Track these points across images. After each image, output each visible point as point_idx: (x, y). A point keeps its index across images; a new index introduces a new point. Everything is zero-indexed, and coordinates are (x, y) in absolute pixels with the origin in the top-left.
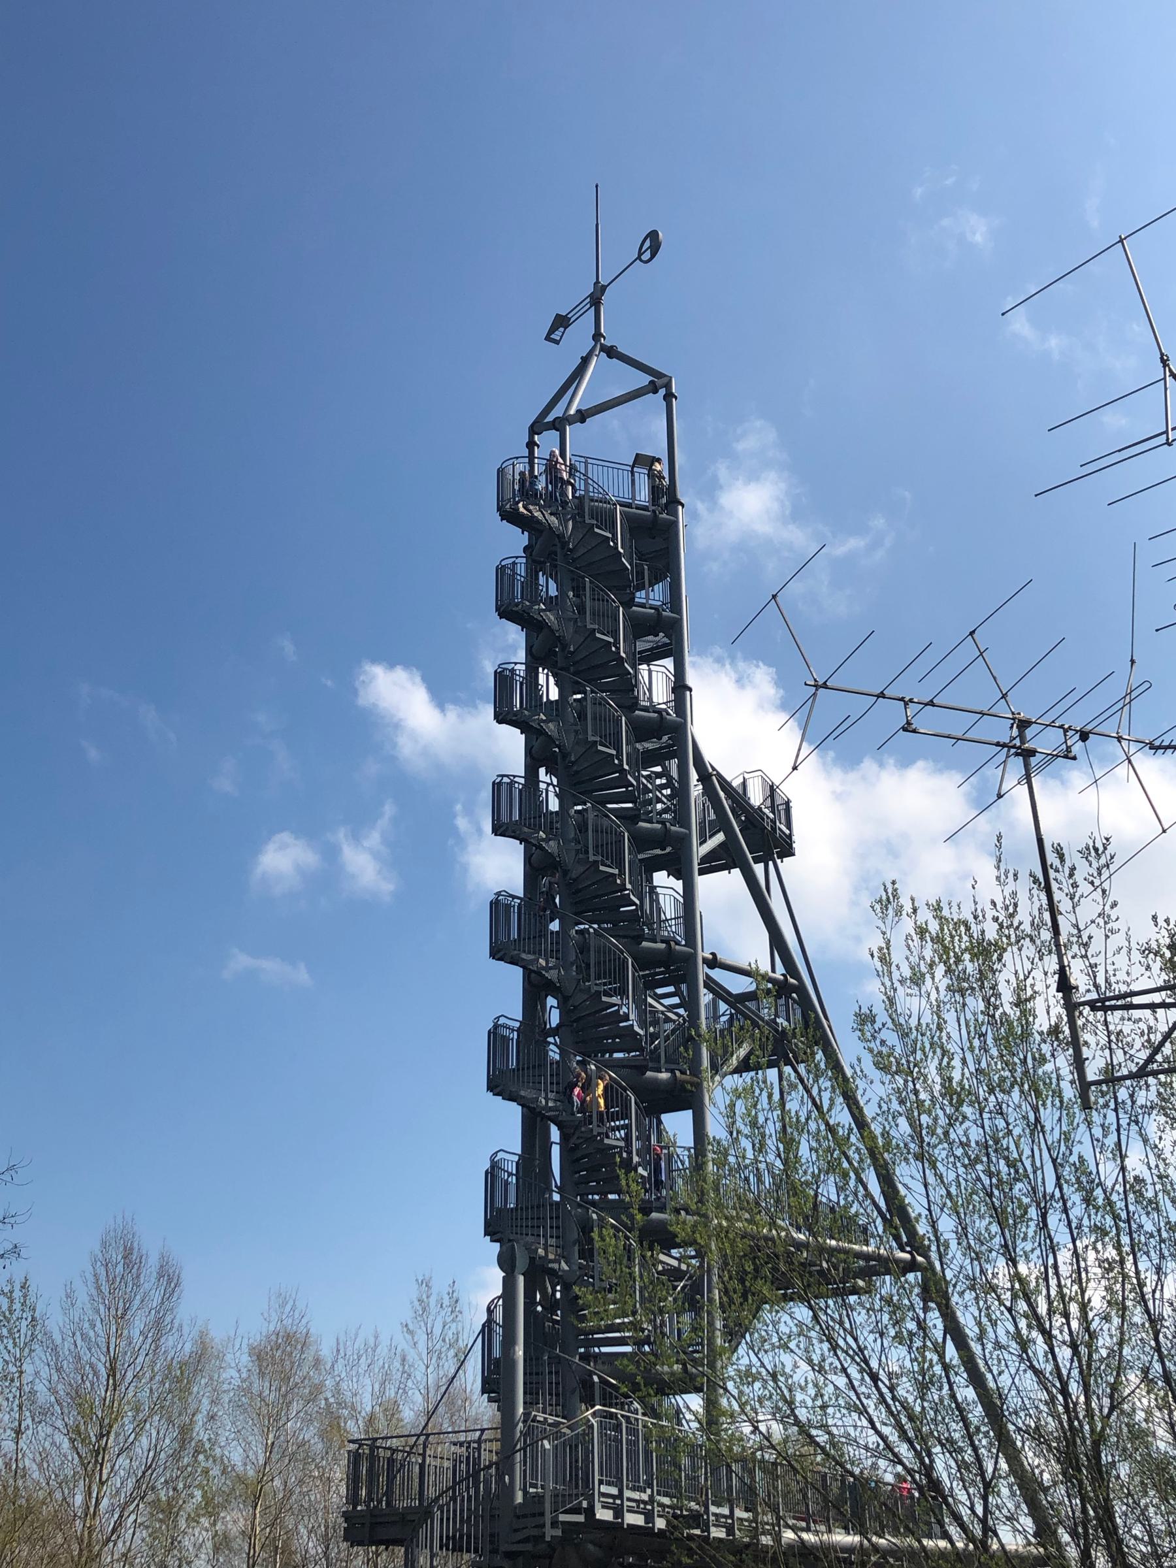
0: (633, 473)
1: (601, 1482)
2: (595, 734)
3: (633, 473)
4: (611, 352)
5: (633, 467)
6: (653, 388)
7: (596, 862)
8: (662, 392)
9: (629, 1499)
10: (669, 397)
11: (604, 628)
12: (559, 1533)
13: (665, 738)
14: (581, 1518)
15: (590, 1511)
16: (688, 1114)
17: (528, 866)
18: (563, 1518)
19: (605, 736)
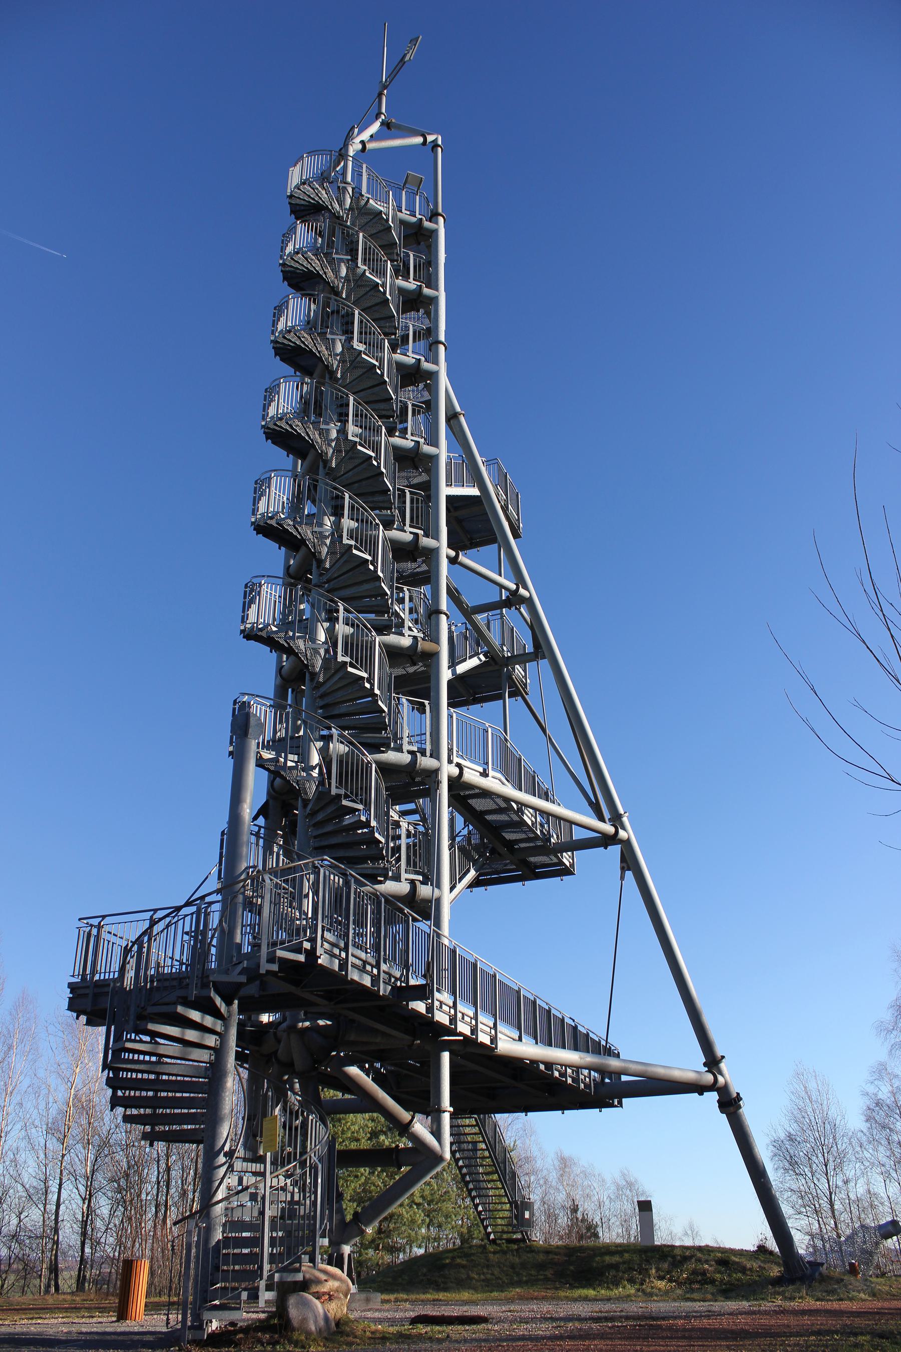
12: (275, 967)
14: (301, 958)
18: (281, 953)
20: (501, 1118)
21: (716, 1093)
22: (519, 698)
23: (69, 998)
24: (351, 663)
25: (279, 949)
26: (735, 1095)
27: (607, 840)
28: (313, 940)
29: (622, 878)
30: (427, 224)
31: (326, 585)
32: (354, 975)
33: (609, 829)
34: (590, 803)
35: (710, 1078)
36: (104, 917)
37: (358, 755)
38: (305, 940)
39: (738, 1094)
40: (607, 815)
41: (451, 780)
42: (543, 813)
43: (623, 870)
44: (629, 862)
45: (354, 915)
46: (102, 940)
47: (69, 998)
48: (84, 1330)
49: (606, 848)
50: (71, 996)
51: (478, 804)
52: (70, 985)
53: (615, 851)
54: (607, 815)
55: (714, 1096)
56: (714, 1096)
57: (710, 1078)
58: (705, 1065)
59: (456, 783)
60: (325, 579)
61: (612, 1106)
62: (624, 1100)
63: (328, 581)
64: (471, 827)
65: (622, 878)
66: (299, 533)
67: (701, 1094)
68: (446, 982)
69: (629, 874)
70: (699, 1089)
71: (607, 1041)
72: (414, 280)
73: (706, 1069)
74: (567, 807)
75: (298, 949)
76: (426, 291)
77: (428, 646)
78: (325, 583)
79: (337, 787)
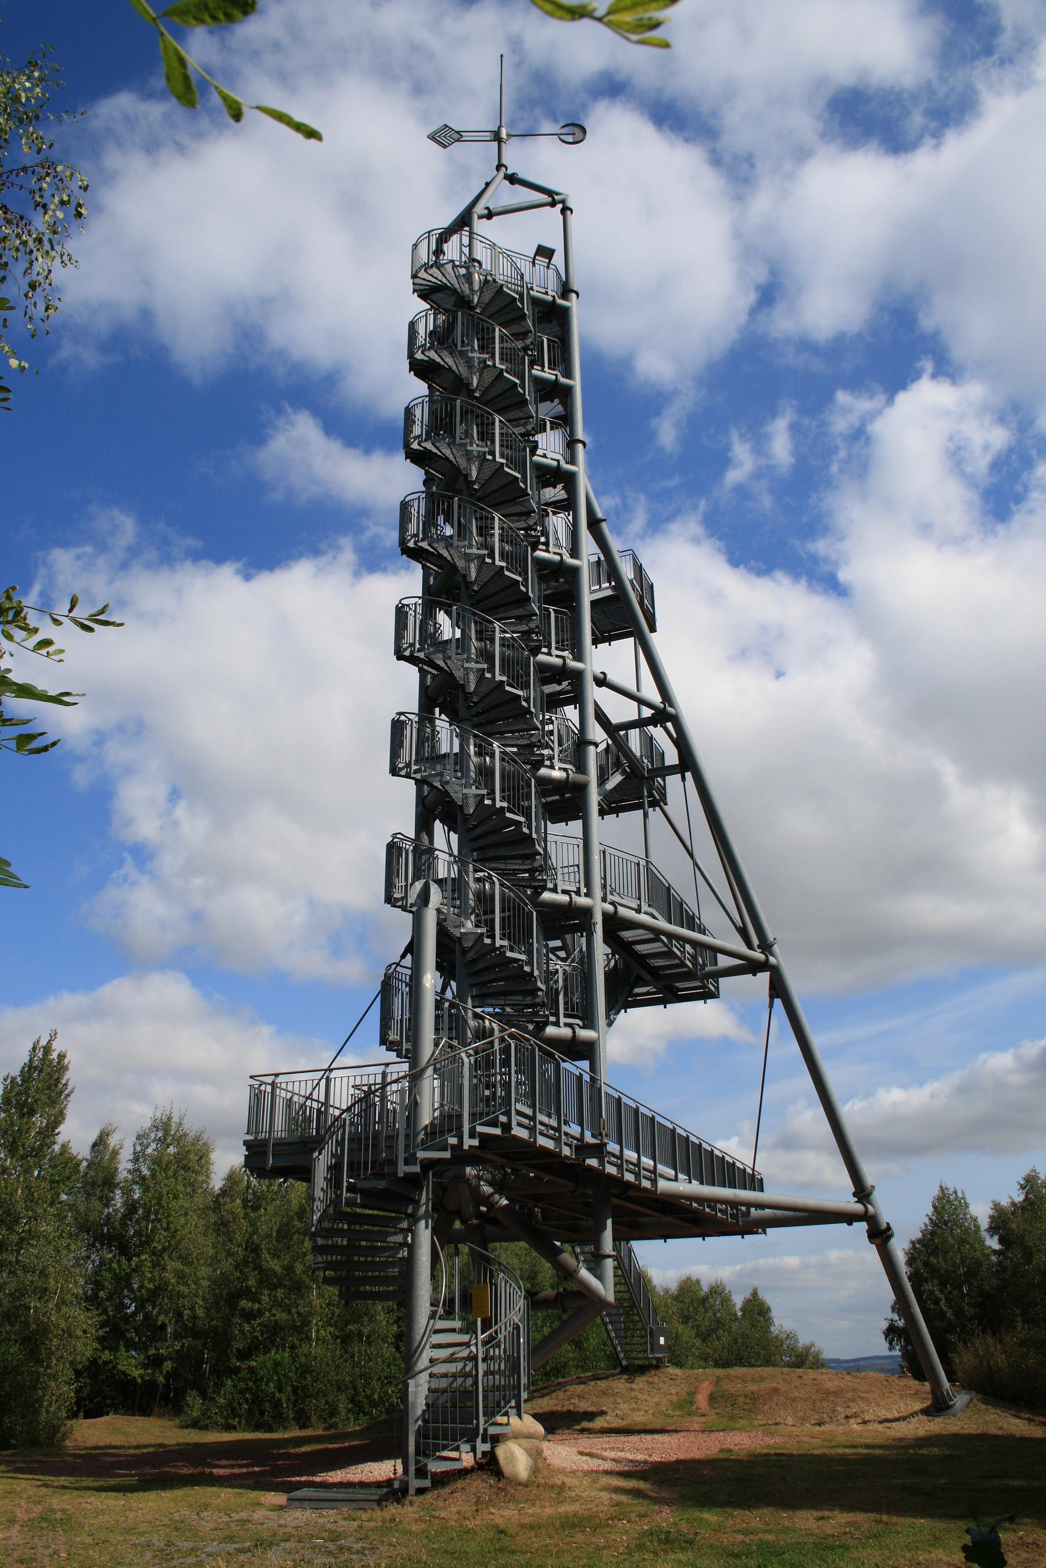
0: (534, 264)
1: (517, 1101)
2: (503, 799)
3: (534, 264)
4: (512, 179)
5: (534, 259)
6: (553, 204)
7: (502, 808)
8: (560, 206)
9: (541, 1123)
10: (565, 210)
11: (514, 806)
12: (475, 1142)
13: (565, 683)
14: (497, 1131)
15: (507, 1127)
16: (579, 823)
17: (421, 807)
18: (480, 1129)
19: (513, 677)
20: (635, 1245)
21: (865, 1224)
22: (657, 808)
23: (246, 1156)
24: (508, 807)
25: (480, 1124)
26: (884, 1226)
27: (752, 967)
28: (508, 1113)
29: (771, 1006)
30: (560, 302)
31: (475, 719)
32: (542, 1141)
33: (758, 955)
34: (738, 929)
35: (859, 1208)
36: (277, 1075)
37: (519, 905)
38: (501, 1114)
39: (888, 1224)
40: (756, 942)
41: (606, 916)
42: (694, 944)
43: (772, 997)
44: (778, 989)
45: (516, 1066)
46: (278, 1098)
47: (246, 1156)
48: (351, 1490)
49: (755, 975)
50: (247, 1153)
51: (628, 935)
52: (246, 1143)
53: (764, 977)
54: (756, 942)
55: (863, 1226)
56: (863, 1226)
57: (859, 1208)
58: (855, 1194)
59: (607, 918)
60: (474, 712)
61: (757, 1233)
62: (768, 1230)
63: (478, 714)
64: (617, 957)
65: (771, 1006)
66: (449, 667)
67: (850, 1224)
68: (613, 1132)
69: (778, 1002)
70: (848, 1218)
71: (753, 1170)
72: (549, 368)
73: (856, 1199)
74: (912, 1286)
75: (493, 1123)
76: (563, 380)
77: (580, 777)
78: (474, 716)
79: (501, 939)
